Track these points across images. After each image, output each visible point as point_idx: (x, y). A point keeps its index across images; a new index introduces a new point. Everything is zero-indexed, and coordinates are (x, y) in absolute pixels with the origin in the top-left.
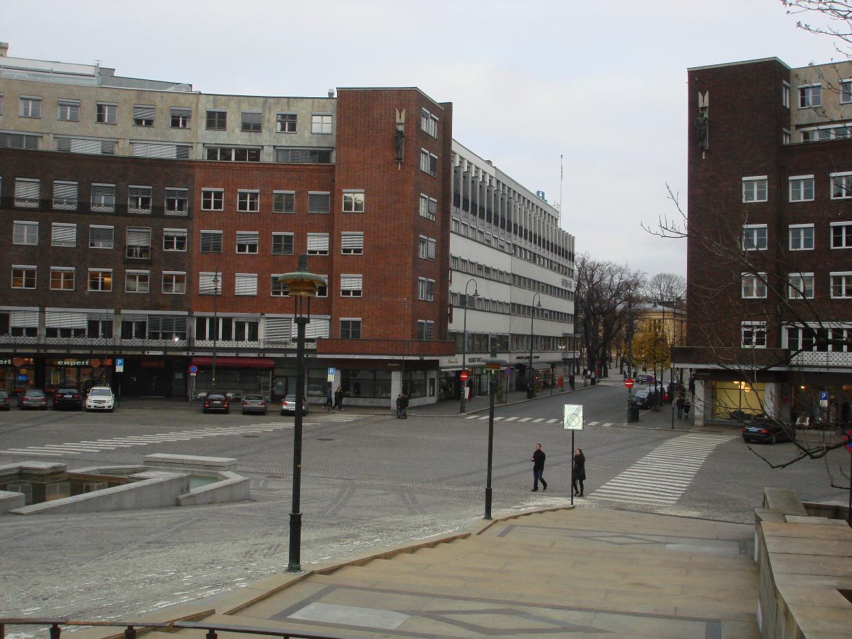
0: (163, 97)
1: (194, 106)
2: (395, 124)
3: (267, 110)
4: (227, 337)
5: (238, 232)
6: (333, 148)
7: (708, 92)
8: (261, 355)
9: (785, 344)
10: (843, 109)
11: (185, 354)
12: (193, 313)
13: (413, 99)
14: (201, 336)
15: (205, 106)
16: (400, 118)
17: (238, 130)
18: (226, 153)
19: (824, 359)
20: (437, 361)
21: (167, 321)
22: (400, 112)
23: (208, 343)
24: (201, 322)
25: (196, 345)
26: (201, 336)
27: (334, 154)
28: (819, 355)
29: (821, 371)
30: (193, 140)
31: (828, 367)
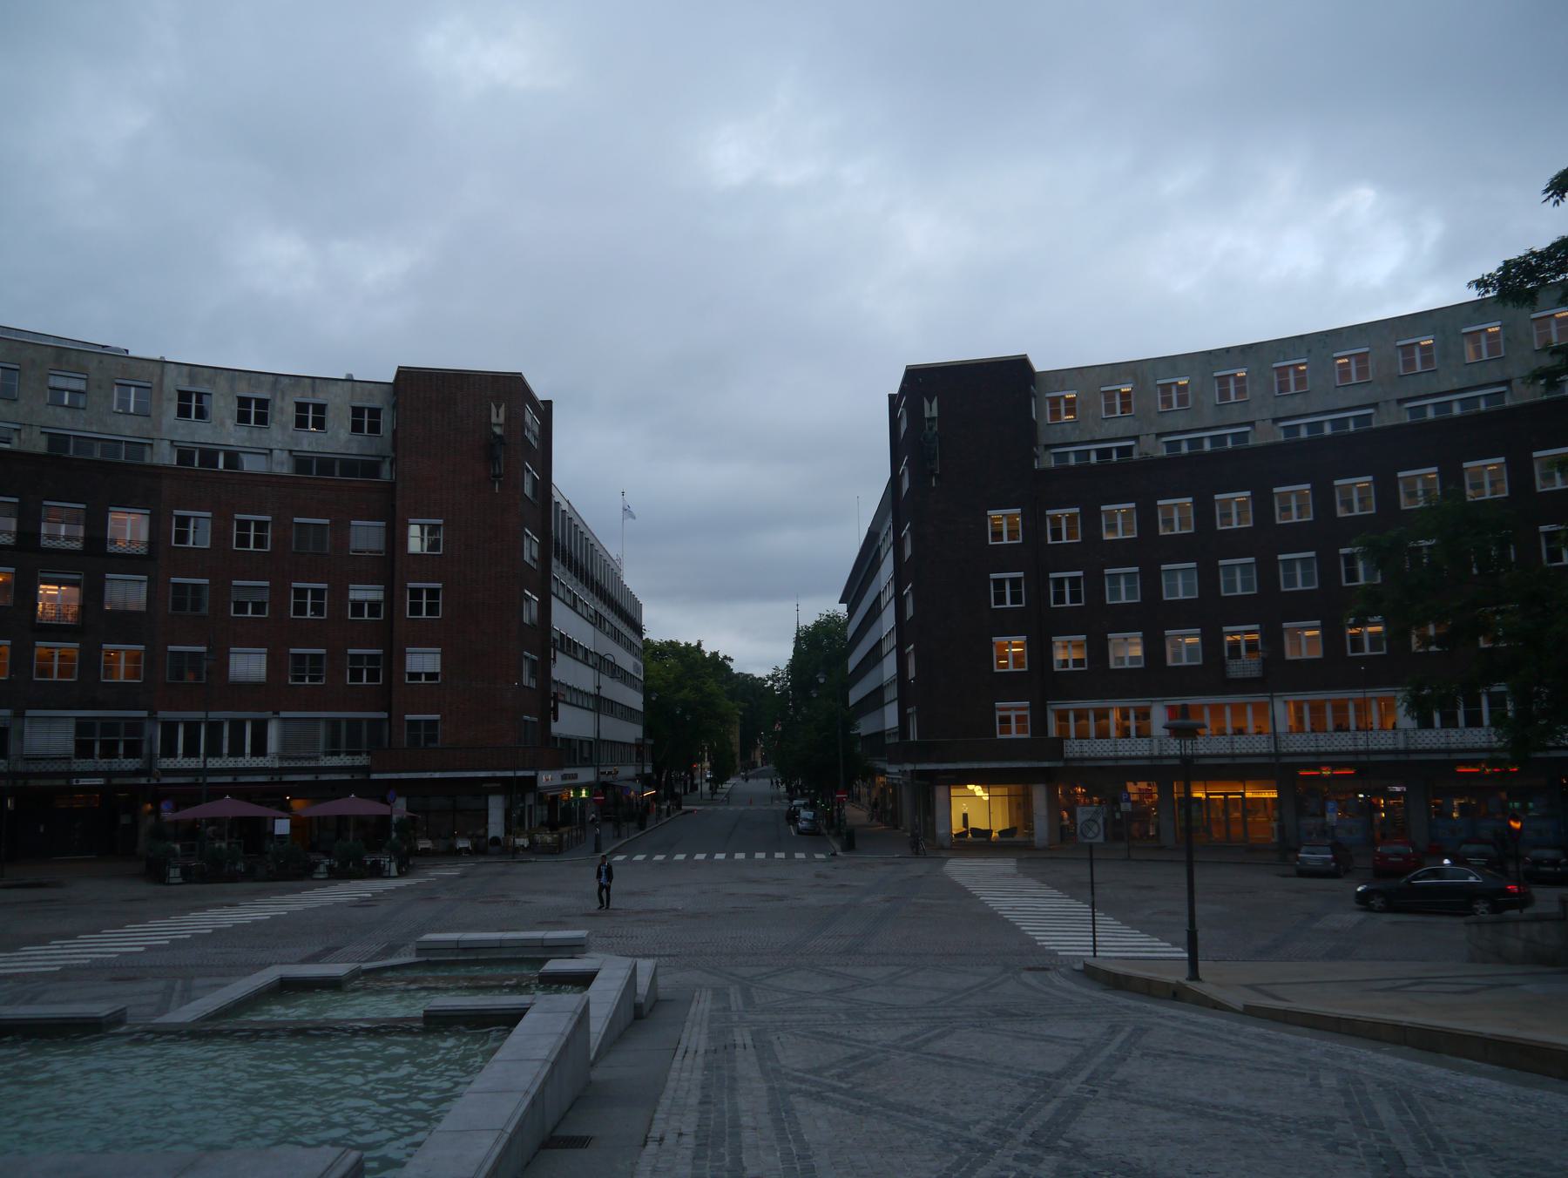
0: (101, 362)
1: (155, 380)
2: (489, 424)
3: (279, 394)
4: (191, 751)
5: (235, 583)
6: (384, 457)
7: (936, 398)
8: (276, 779)
9: (1053, 731)
10: (1107, 424)
11: (143, 781)
12: (156, 713)
13: (511, 388)
14: (169, 751)
15: (175, 383)
16: (498, 416)
17: (230, 423)
18: (209, 456)
19: (1146, 748)
20: (534, 779)
21: (110, 726)
22: (498, 407)
23: (182, 762)
24: (169, 729)
25: (896, 723)
26: (169, 751)
27: (386, 467)
28: (1139, 742)
29: (1154, 763)
30: (154, 435)
31: (1117, 759)
